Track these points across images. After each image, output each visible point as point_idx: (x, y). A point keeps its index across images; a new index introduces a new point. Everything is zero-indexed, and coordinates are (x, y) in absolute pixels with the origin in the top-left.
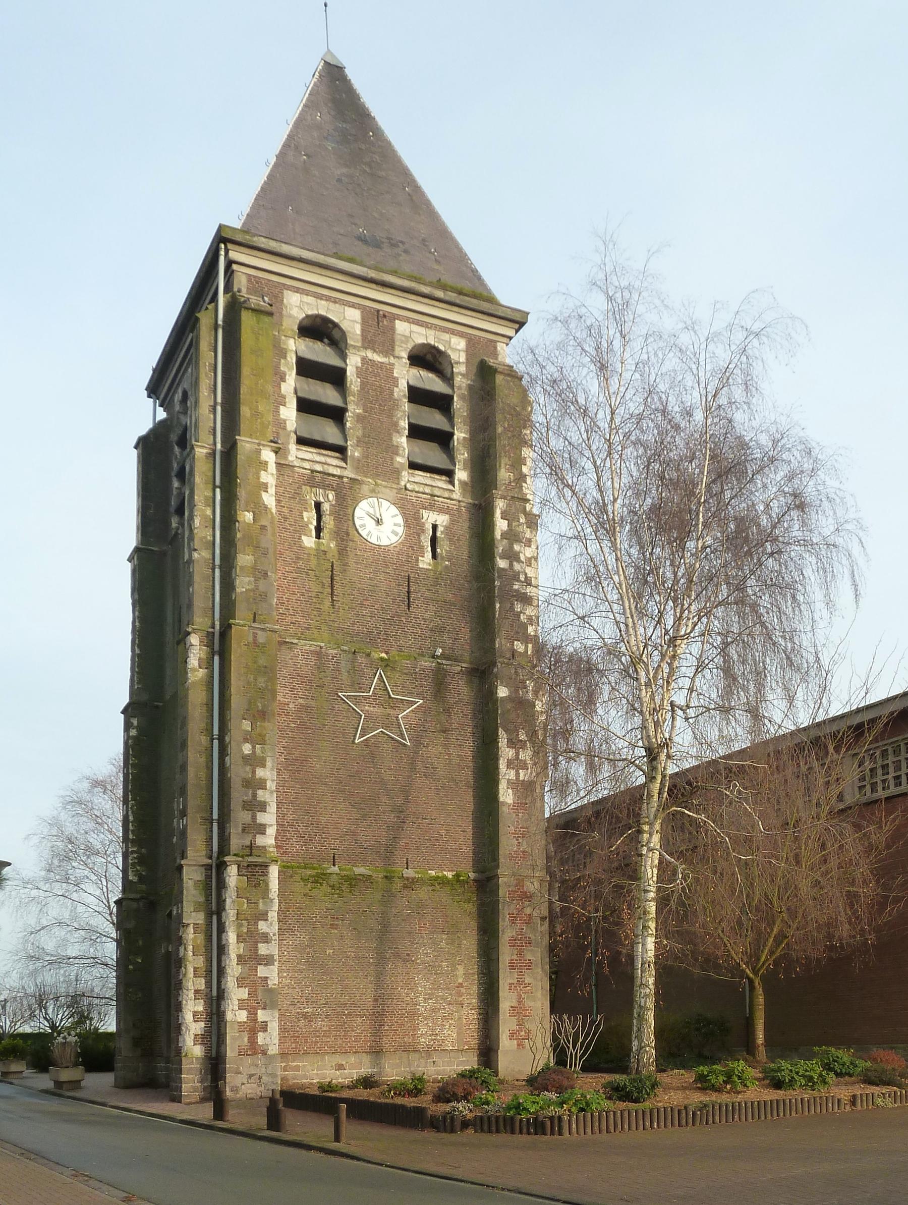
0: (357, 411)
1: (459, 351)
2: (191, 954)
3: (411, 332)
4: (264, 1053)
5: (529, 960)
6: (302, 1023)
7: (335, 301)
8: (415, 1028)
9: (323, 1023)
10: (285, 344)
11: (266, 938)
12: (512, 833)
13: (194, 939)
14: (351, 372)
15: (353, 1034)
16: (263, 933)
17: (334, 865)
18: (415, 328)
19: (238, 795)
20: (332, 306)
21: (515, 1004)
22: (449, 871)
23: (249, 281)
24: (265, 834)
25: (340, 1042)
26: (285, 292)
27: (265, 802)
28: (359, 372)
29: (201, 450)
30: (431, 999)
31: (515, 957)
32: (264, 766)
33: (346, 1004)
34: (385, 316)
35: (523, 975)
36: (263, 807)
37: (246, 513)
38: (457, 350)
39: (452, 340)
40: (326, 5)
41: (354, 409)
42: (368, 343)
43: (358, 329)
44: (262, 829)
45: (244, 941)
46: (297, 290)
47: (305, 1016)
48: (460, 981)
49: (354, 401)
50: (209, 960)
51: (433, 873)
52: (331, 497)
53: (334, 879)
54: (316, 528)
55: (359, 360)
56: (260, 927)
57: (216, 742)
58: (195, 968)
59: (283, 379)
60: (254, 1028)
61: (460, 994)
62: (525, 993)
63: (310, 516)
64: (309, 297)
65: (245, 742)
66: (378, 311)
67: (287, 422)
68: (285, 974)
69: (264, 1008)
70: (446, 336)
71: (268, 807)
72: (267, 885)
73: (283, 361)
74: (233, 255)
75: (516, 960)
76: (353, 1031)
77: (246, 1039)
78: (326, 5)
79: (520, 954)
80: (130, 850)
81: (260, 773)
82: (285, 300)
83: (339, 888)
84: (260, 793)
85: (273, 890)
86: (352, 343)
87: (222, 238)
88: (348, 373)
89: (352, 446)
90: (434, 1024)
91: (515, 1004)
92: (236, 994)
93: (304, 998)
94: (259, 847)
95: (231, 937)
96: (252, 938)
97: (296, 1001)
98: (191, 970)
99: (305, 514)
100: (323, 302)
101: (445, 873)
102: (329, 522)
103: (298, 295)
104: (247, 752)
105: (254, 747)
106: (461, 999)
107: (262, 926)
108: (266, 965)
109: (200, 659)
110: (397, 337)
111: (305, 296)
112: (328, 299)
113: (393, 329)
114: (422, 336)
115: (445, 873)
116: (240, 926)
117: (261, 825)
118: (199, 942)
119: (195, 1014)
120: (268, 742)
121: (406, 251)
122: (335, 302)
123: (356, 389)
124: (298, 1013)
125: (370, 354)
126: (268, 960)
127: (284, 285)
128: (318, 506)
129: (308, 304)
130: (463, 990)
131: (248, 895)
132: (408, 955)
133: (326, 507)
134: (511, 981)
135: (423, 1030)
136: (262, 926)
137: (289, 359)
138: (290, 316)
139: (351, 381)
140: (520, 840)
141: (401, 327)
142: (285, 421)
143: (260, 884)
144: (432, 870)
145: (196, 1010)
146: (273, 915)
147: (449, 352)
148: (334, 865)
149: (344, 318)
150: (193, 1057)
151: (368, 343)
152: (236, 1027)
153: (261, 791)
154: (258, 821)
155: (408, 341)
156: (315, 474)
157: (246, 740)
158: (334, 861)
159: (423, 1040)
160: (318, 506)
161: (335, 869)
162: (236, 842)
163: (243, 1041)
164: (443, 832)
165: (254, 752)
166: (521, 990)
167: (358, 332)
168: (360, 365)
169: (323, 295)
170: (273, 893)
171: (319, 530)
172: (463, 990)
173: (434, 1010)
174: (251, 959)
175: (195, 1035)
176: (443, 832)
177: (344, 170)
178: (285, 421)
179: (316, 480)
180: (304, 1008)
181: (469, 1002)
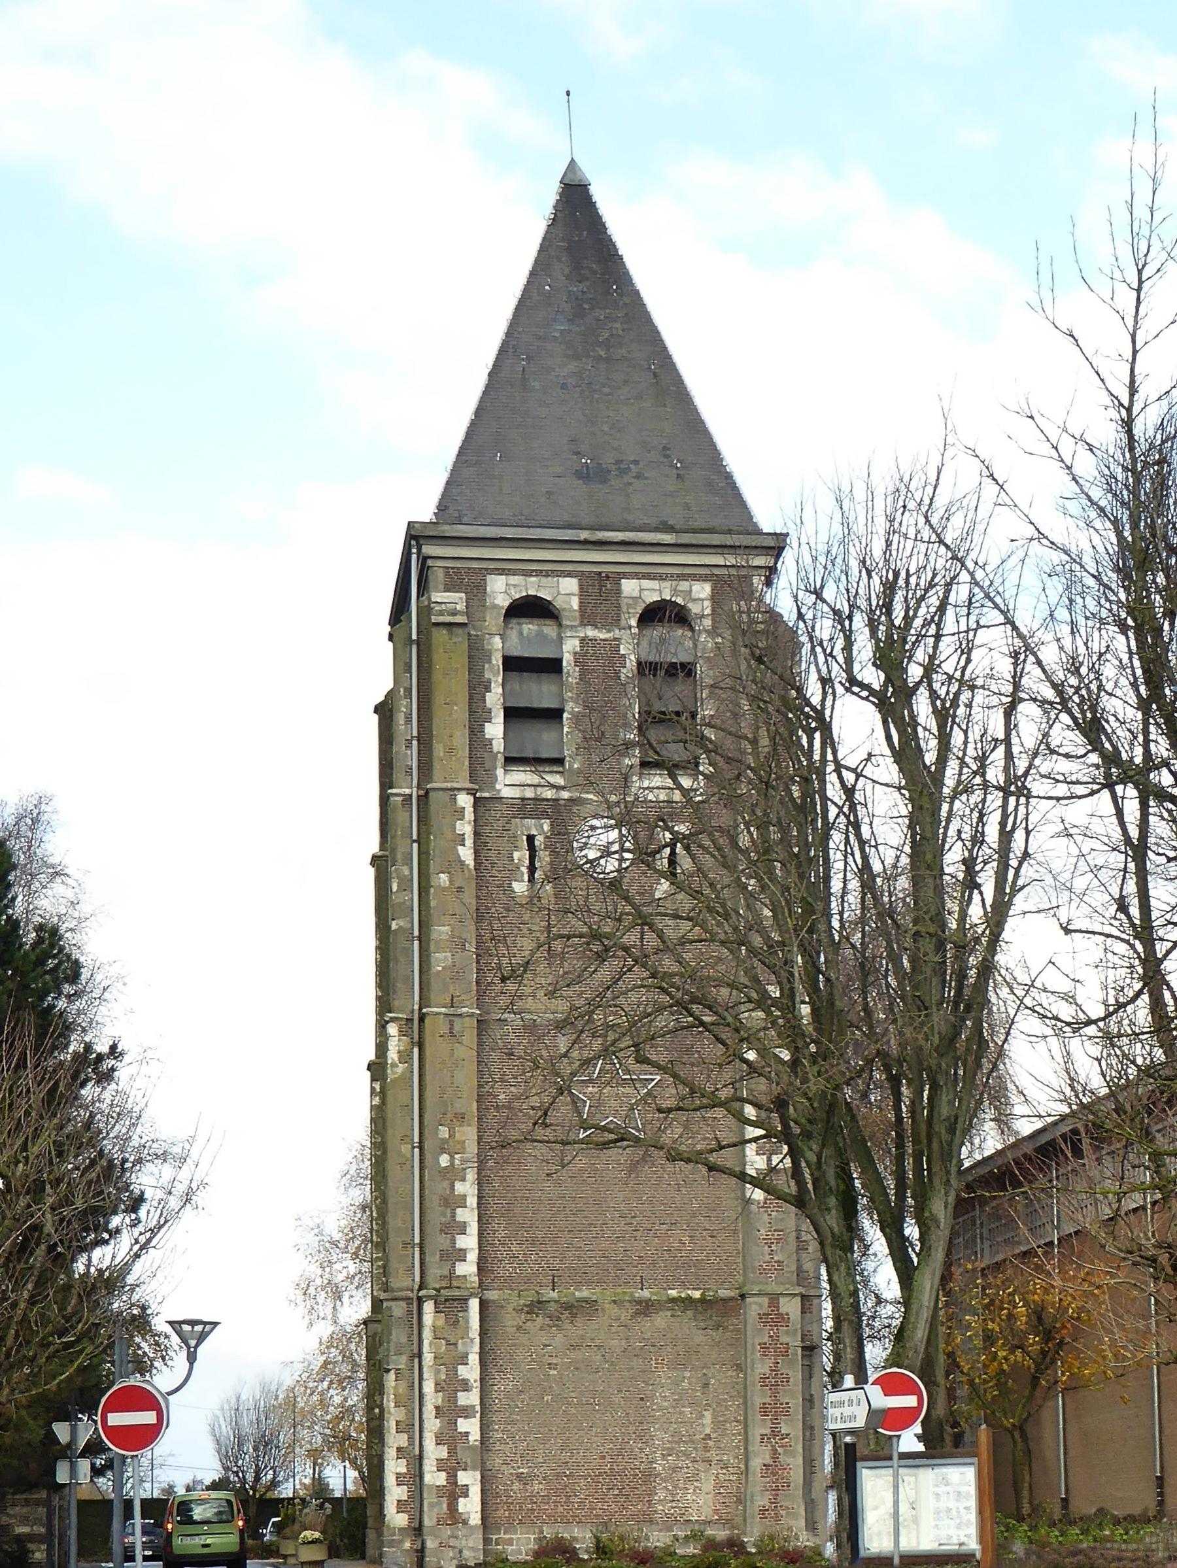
0: (576, 710)
1: (703, 600)
2: (393, 1405)
3: (641, 590)
4: (465, 1522)
5: (787, 1403)
6: (516, 1486)
7: (547, 574)
8: (652, 1493)
9: (541, 1486)
10: (489, 644)
11: (465, 1386)
12: (764, 1239)
13: (395, 1388)
14: (567, 659)
15: (576, 1500)
16: (463, 1380)
17: (554, 1290)
18: (646, 583)
19: (436, 1217)
20: (544, 581)
21: (769, 1461)
22: (694, 1289)
23: (447, 574)
24: (465, 1261)
25: (560, 1509)
26: (489, 577)
27: (465, 1222)
28: (579, 659)
29: (396, 798)
30: (670, 1455)
31: (768, 1400)
32: (463, 1180)
33: (567, 1463)
34: (607, 577)
35: (779, 1423)
36: (462, 1229)
37: (442, 875)
38: (699, 599)
39: (693, 588)
40: (568, 94)
41: (572, 708)
42: (587, 617)
43: (575, 603)
44: (461, 1255)
45: (442, 1390)
46: (502, 572)
47: (519, 1476)
48: (708, 1431)
49: (571, 698)
50: (410, 1412)
51: (673, 1293)
52: (546, 827)
53: (553, 1307)
54: (528, 868)
55: (577, 642)
56: (459, 1373)
57: (417, 1151)
58: (397, 1422)
59: (488, 689)
60: (454, 1492)
61: (706, 1449)
62: (782, 1446)
63: (521, 856)
64: (517, 577)
65: (442, 1153)
66: (600, 573)
67: (494, 742)
68: (497, 1427)
69: (465, 1470)
70: (684, 586)
71: (468, 1229)
72: (467, 1322)
73: (487, 666)
74: (427, 550)
75: (770, 1404)
76: (576, 1496)
77: (445, 1506)
78: (568, 94)
79: (774, 1395)
80: (374, 1256)
81: (460, 1188)
82: (488, 589)
83: (559, 1319)
84: (459, 1211)
85: (474, 1328)
86: (568, 623)
87: (415, 536)
88: (564, 664)
89: (570, 756)
90: (676, 1487)
91: (769, 1461)
92: (434, 1452)
93: (519, 1456)
94: (459, 1276)
95: (429, 1387)
96: (451, 1386)
97: (509, 1459)
98: (393, 1424)
99: (516, 855)
100: (533, 579)
101: (689, 1292)
102: (544, 858)
103: (504, 577)
104: (443, 1165)
105: (452, 1158)
106: (708, 1455)
107: (463, 1371)
108: (466, 1417)
109: (399, 1052)
110: (624, 602)
111: (511, 577)
112: (539, 573)
113: (618, 591)
114: (653, 592)
115: (689, 1292)
116: (437, 1372)
117: (461, 1250)
118: (401, 1390)
119: (398, 1475)
120: (468, 1150)
121: (639, 476)
122: (547, 576)
123: (574, 681)
124: (511, 1474)
125: (591, 632)
126: (466, 1412)
127: (486, 569)
128: (531, 839)
129: (515, 586)
130: (711, 1443)
131: (446, 1336)
132: (642, 1399)
133: (539, 841)
134: (764, 1432)
135: (661, 1494)
136: (463, 1371)
137: (494, 662)
138: (495, 606)
139: (568, 673)
140: (774, 1247)
141: (629, 587)
142: (490, 741)
143: (458, 1321)
144: (673, 1289)
145: (398, 1471)
146: (474, 1358)
147: (690, 605)
148: (554, 1290)
149: (559, 594)
150: (395, 1528)
151: (587, 617)
152: (434, 1491)
153: (460, 1209)
154: (457, 1246)
155: (636, 604)
156: (526, 802)
157: (443, 1151)
158: (554, 1286)
159: (661, 1508)
160: (531, 839)
161: (554, 1295)
162: (435, 1272)
163: (442, 1508)
164: (686, 1240)
165: (452, 1164)
166: (776, 1443)
167: (576, 607)
168: (578, 649)
169: (533, 571)
170: (474, 1331)
171: (532, 869)
172: (711, 1443)
173: (675, 1469)
174: (450, 1412)
175: (398, 1501)
176: (686, 1240)
177: (572, 366)
178: (490, 741)
179: (528, 808)
180: (519, 1467)
181: (718, 1458)
